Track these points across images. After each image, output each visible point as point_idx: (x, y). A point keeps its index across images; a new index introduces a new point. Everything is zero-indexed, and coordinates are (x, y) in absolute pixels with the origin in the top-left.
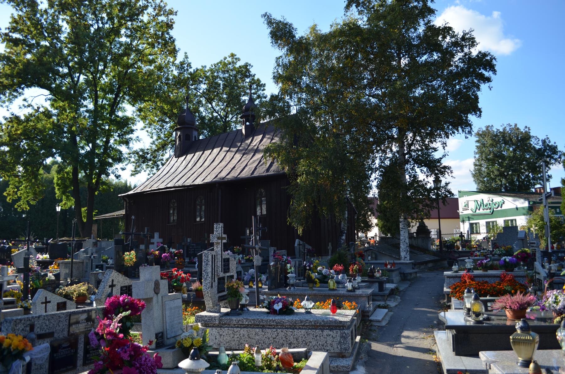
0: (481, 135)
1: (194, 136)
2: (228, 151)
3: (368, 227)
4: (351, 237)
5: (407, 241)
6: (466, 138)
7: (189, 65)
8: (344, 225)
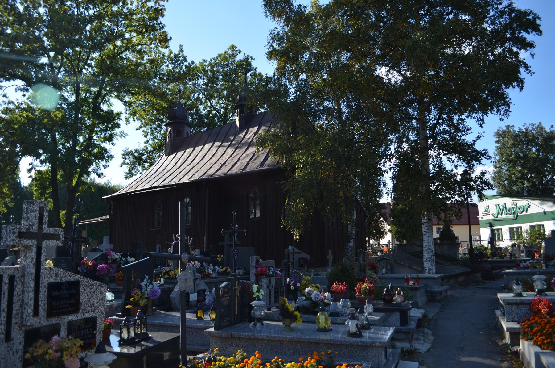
0: (500, 135)
1: (185, 132)
2: (219, 147)
3: (381, 234)
4: (361, 245)
5: (432, 248)
6: (501, 120)
7: (185, 59)
8: (352, 230)
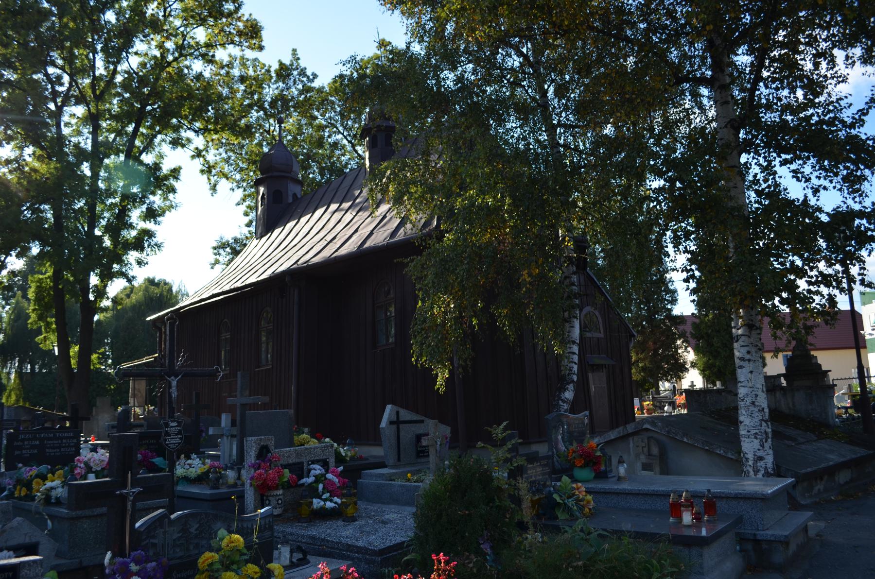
1: (290, 194)
3: (678, 369)
5: (763, 401)
